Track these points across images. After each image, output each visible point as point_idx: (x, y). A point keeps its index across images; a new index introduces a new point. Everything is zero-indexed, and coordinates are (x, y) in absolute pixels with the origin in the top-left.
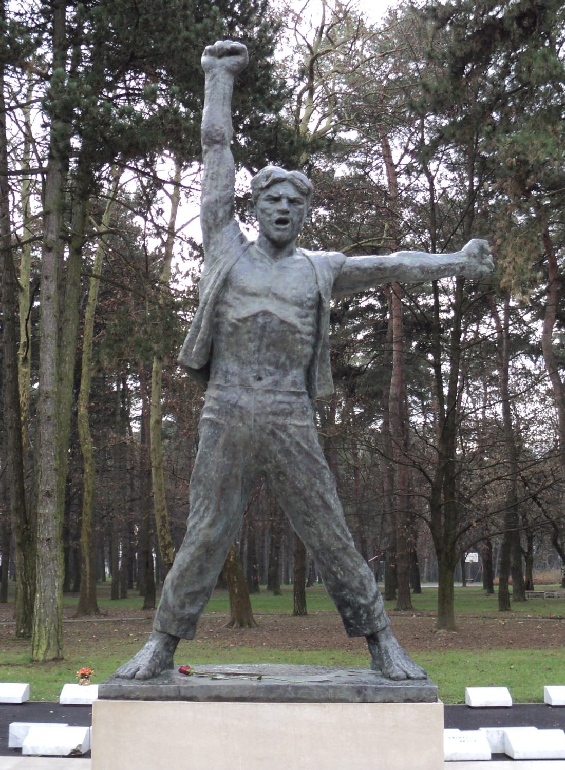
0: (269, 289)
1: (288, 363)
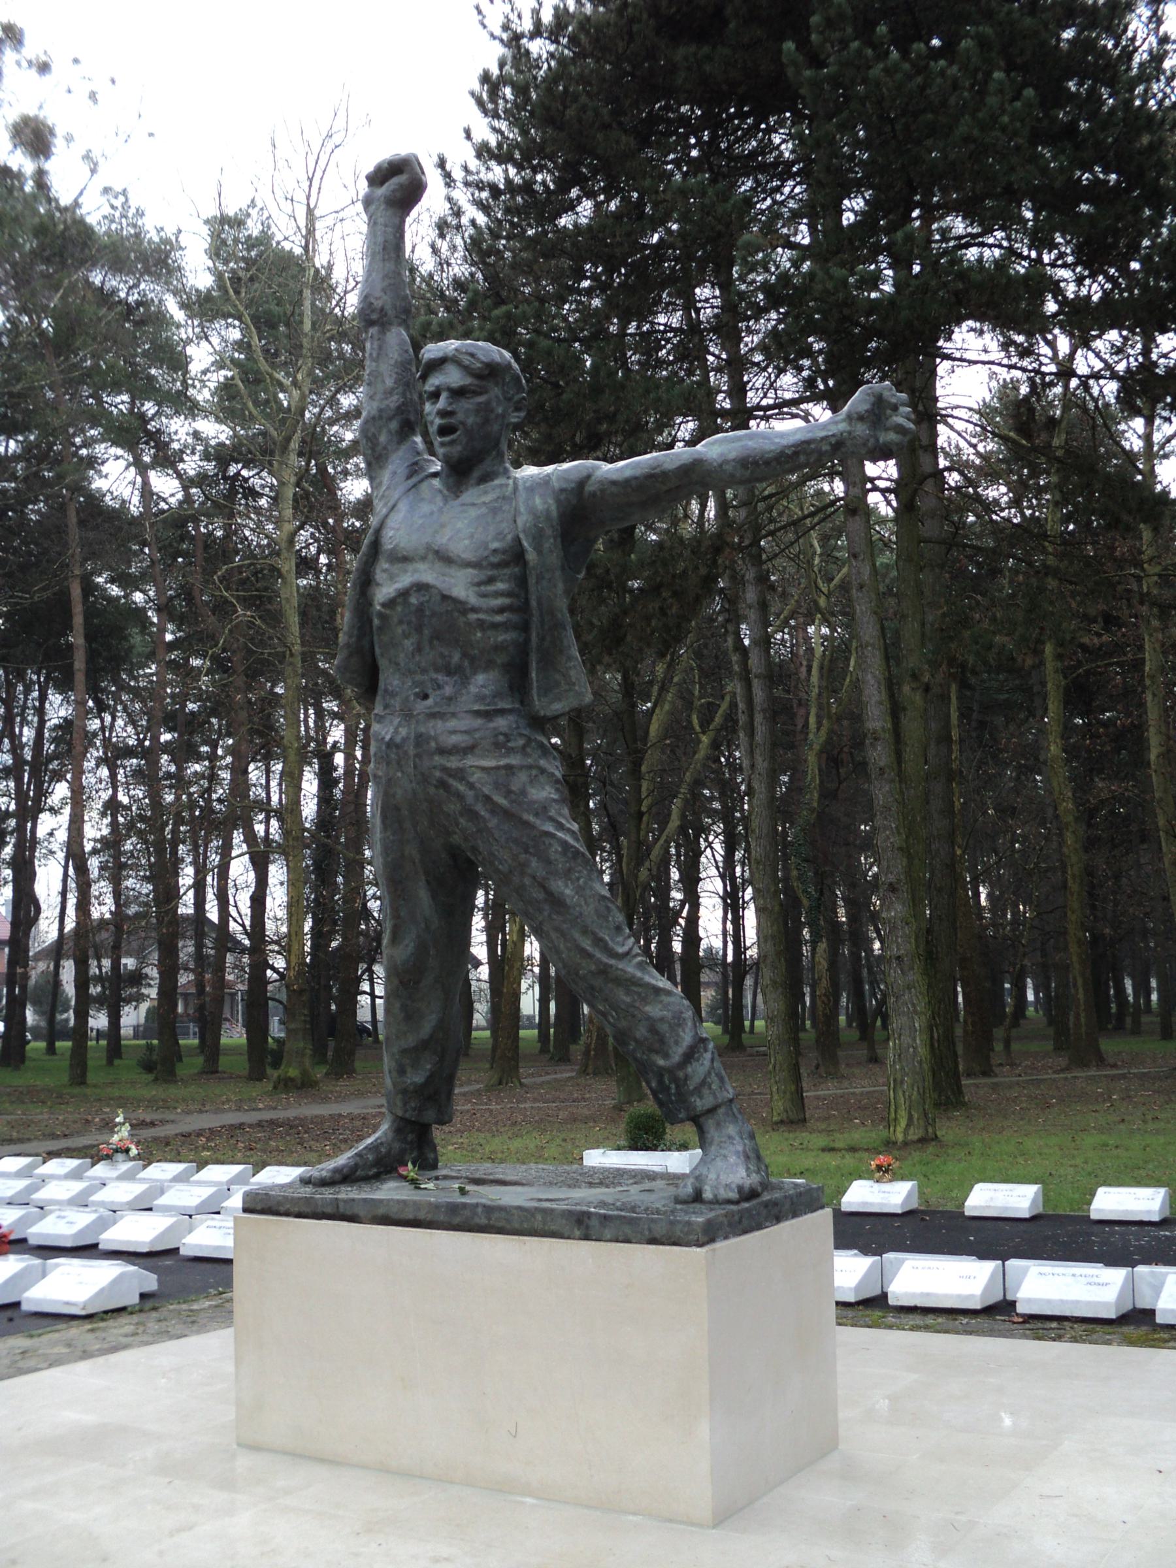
0: (429, 548)
1: (466, 663)
